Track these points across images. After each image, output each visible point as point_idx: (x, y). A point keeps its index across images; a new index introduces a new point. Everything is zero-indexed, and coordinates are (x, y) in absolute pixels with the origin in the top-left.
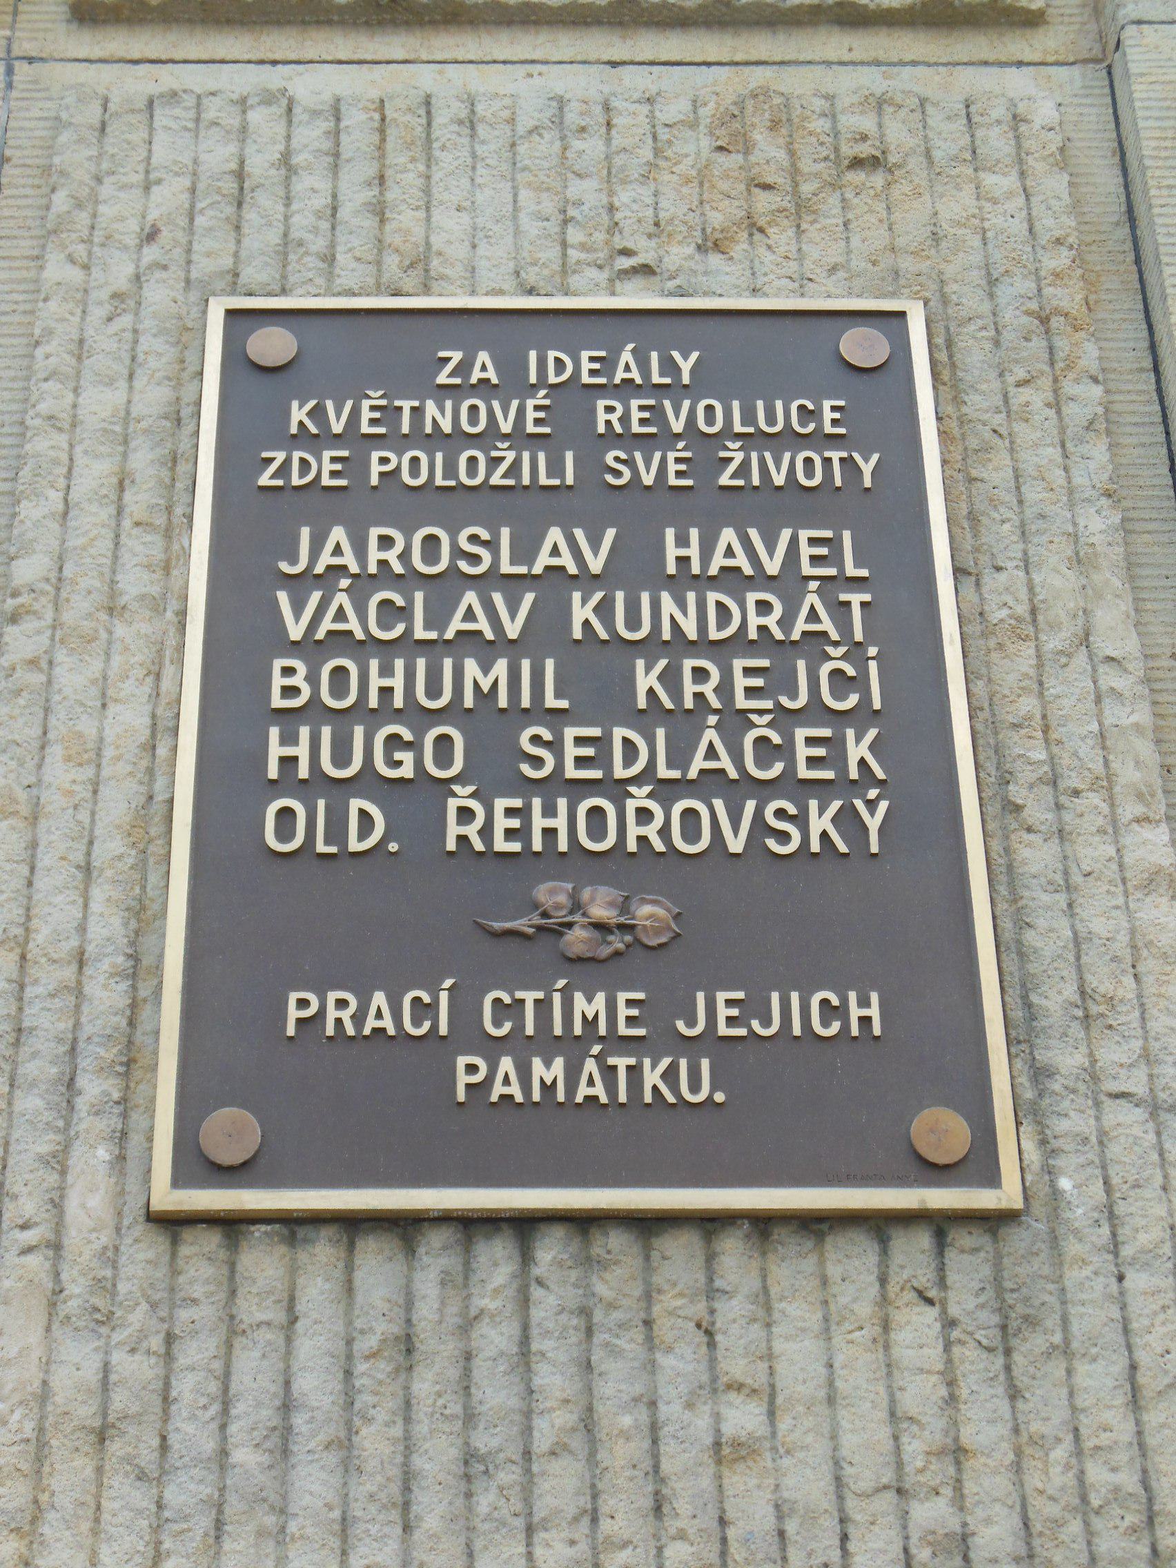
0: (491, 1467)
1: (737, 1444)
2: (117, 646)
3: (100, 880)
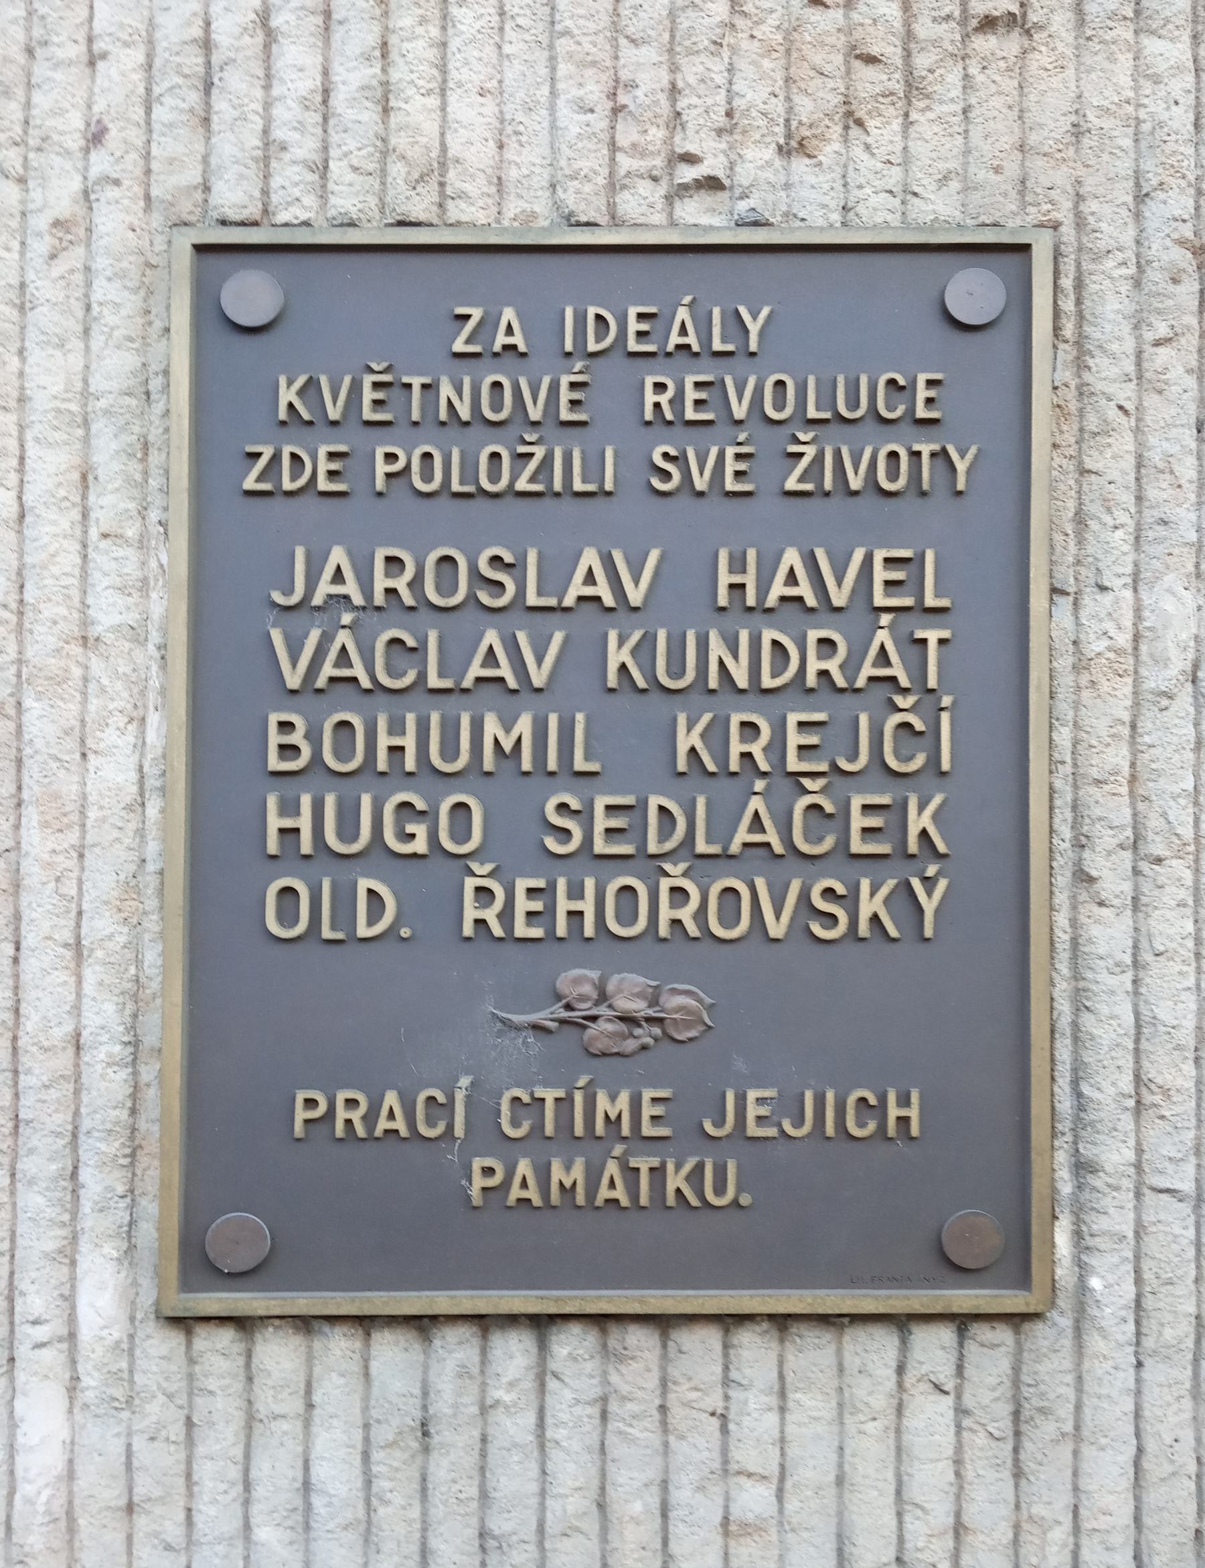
0: (504, 1545)
1: (744, 1525)
2: (92, 687)
3: (90, 960)
